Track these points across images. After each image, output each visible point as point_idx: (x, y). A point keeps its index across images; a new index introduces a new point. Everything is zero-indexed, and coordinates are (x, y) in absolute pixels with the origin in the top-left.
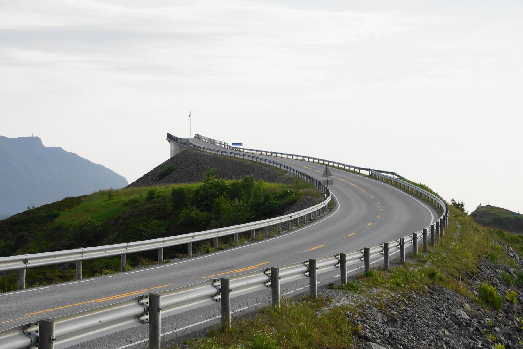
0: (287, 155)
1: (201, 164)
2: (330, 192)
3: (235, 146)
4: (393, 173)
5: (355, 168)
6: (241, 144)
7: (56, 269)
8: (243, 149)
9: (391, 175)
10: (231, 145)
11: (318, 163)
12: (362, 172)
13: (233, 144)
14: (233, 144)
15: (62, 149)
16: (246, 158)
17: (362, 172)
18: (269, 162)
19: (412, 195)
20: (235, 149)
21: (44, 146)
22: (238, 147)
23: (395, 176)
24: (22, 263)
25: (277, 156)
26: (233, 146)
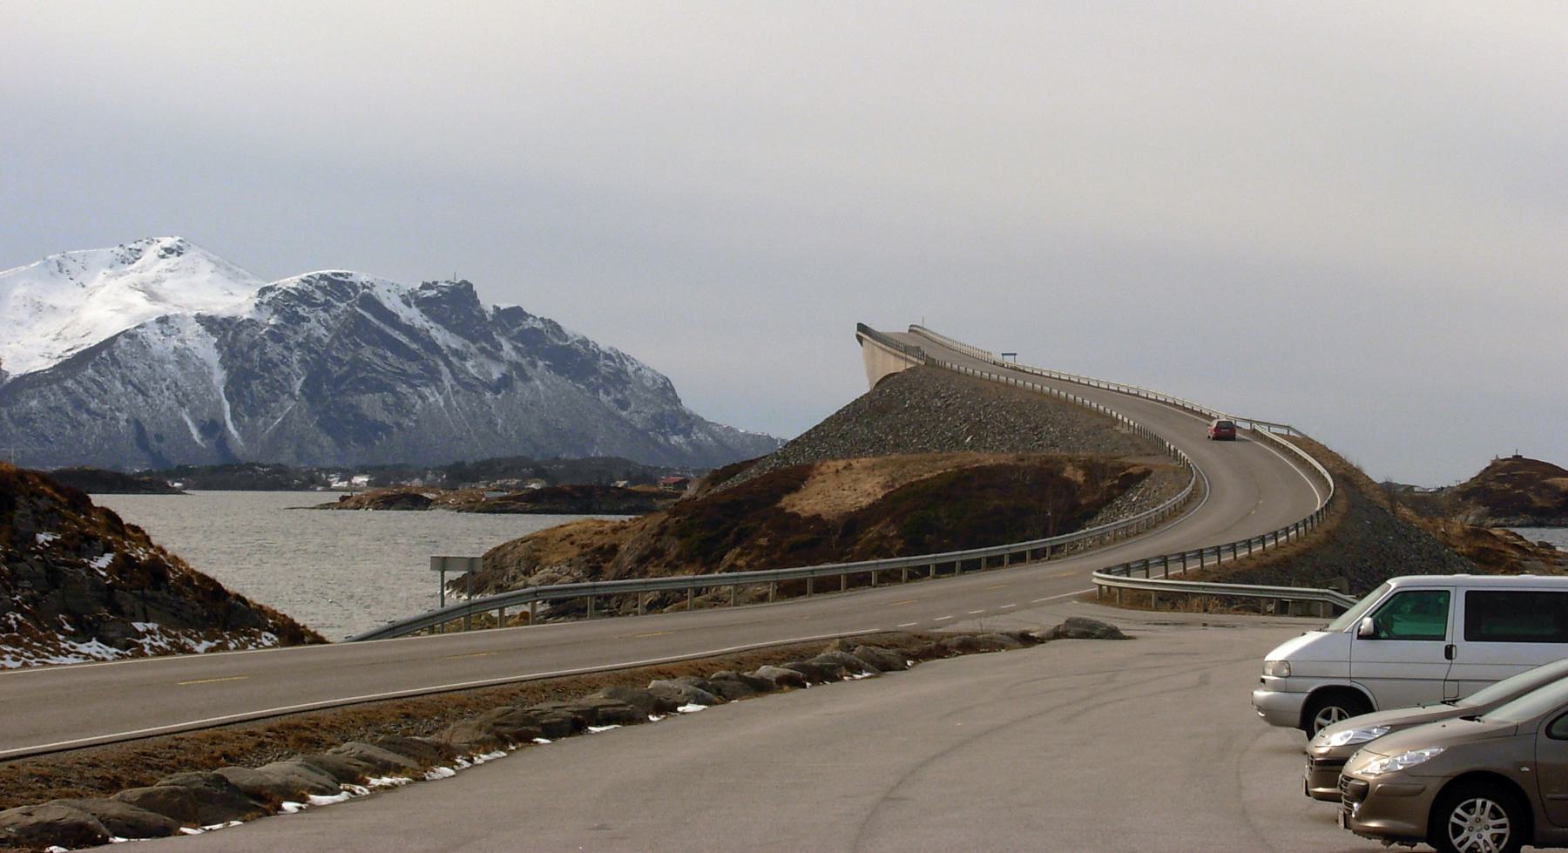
1: (951, 396)
4: (1288, 428)
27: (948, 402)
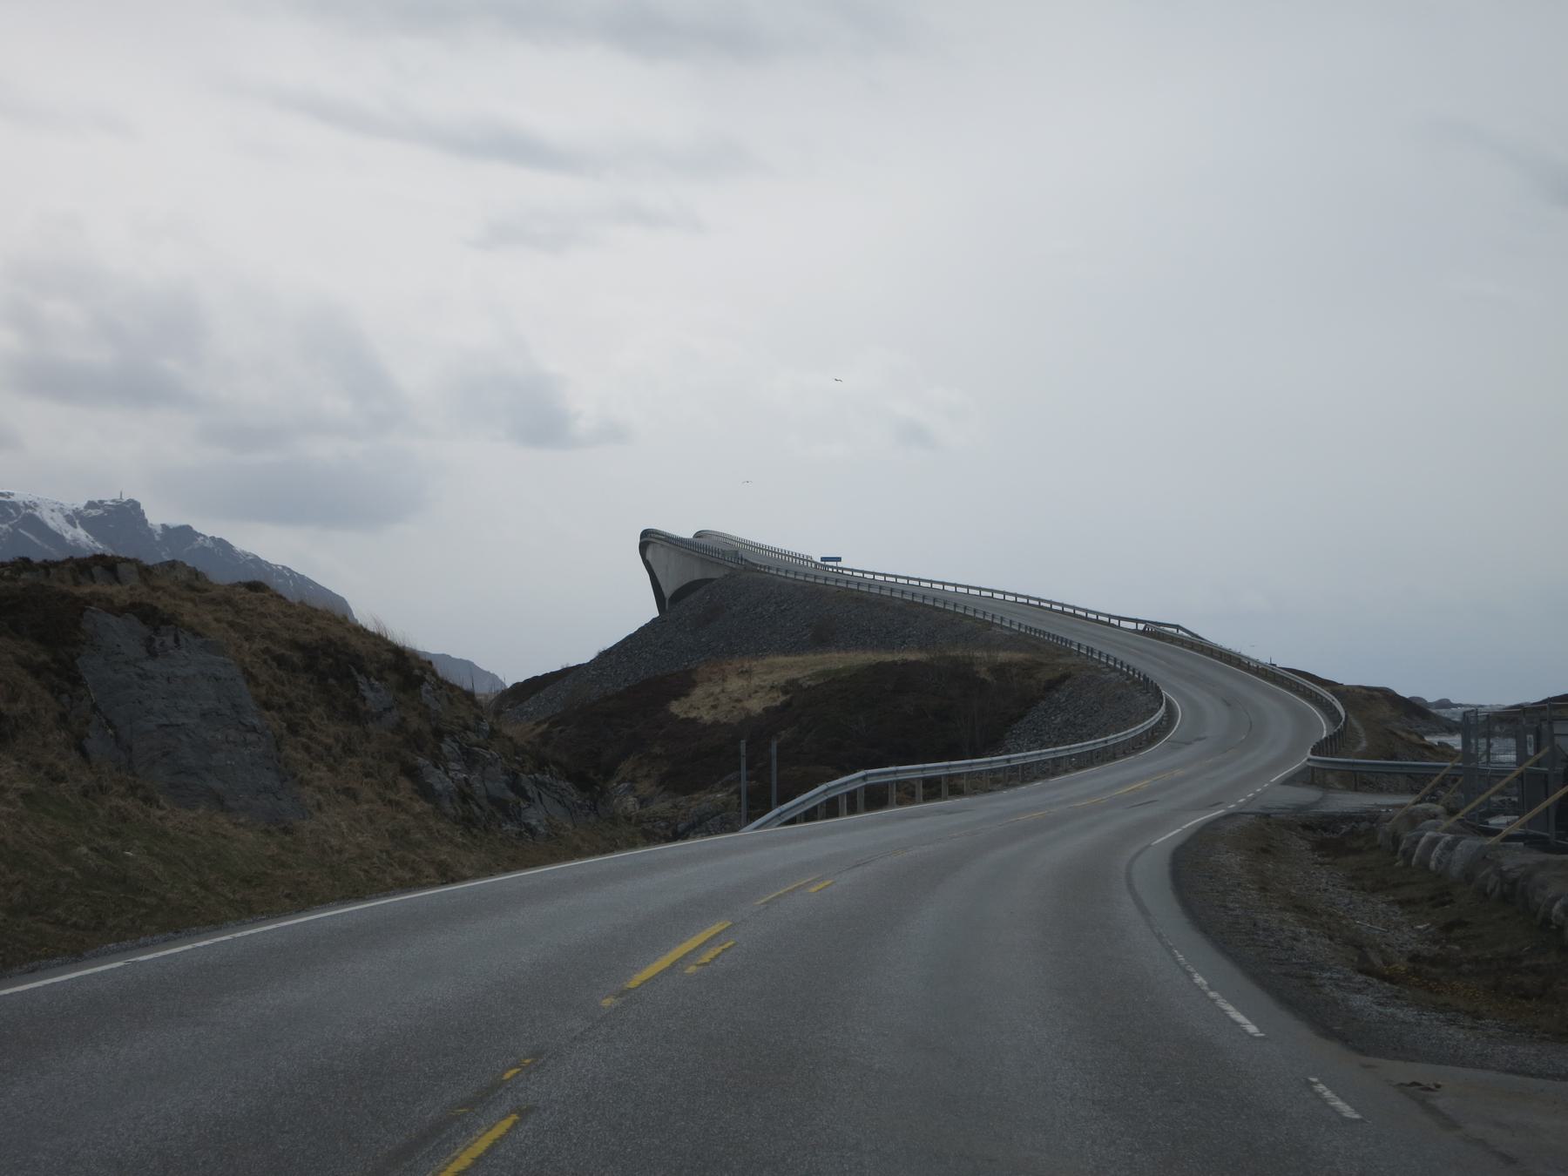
0: (1004, 593)
2: (1163, 691)
3: (827, 563)
4: (1178, 627)
5: (1110, 617)
6: (839, 559)
7: (809, 686)
8: (843, 569)
9: (1175, 630)
10: (819, 561)
11: (1028, 603)
12: (1124, 624)
13: (823, 559)
14: (823, 559)
15: (518, 683)
16: (897, 596)
17: (1124, 624)
18: (787, 572)
19: (1296, 695)
20: (830, 570)
21: (691, 536)
22: (834, 564)
23: (1180, 632)
24: (861, 780)
25: (896, 582)
26: (823, 563)
27: (783, 608)
